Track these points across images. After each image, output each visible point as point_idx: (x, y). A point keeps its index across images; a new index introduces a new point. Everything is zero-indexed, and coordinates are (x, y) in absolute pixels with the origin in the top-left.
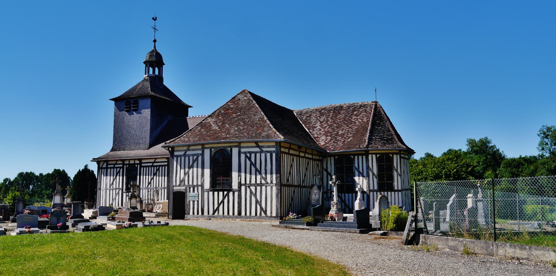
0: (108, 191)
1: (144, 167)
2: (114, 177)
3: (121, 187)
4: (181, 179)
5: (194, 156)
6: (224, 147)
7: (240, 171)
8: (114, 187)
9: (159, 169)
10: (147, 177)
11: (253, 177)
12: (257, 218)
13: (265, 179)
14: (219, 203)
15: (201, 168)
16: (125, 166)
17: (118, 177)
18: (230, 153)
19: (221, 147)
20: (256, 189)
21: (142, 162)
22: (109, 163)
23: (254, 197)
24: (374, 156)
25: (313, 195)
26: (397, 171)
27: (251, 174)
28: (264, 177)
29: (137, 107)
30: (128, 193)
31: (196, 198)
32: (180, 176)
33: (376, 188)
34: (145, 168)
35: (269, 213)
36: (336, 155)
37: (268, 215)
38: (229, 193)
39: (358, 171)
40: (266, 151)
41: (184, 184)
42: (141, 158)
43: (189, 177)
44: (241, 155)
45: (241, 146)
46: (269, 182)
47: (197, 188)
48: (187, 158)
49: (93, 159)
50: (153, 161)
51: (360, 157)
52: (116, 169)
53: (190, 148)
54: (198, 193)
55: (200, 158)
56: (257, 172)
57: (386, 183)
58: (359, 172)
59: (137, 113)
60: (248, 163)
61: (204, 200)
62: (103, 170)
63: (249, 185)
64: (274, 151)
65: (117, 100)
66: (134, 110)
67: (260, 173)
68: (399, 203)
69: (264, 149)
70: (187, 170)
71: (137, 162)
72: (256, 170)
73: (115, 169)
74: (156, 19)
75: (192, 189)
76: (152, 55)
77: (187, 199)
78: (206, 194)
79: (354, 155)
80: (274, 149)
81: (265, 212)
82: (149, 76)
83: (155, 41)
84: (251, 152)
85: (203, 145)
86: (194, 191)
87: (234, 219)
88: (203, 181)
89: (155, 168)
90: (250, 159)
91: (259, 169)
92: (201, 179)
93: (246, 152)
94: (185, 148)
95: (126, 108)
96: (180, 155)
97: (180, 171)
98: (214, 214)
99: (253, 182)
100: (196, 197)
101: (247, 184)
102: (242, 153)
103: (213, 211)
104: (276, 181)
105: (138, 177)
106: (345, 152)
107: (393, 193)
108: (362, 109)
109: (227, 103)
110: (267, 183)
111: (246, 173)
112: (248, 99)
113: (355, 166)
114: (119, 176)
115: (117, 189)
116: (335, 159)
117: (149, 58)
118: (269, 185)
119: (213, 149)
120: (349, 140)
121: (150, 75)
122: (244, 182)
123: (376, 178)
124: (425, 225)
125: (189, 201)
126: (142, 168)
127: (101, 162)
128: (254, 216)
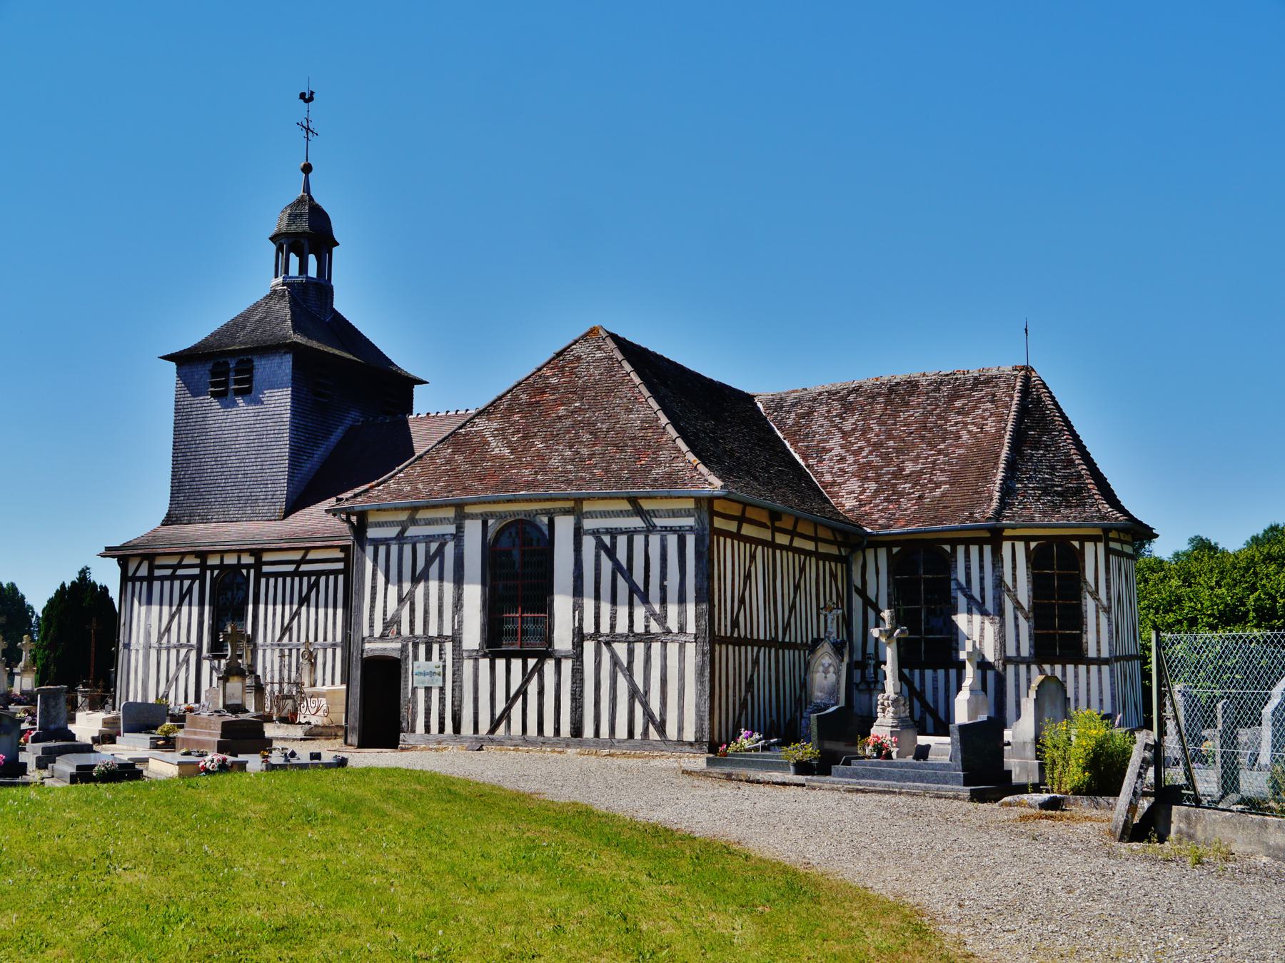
0: (153, 653)
1: (268, 575)
2: (174, 608)
3: (194, 640)
4: (389, 617)
5: (431, 542)
6: (528, 513)
7: (578, 592)
8: (174, 640)
9: (317, 584)
10: (279, 608)
11: (623, 611)
12: (634, 748)
13: (662, 619)
14: (512, 695)
15: (454, 582)
17: (185, 609)
18: (547, 532)
19: (518, 513)
20: (631, 653)
21: (264, 559)
22: (159, 561)
24: (1020, 546)
25: (818, 672)
27: (614, 601)
28: (658, 611)
29: (249, 381)
32: (385, 607)
33: (1025, 651)
34: (272, 581)
35: (672, 732)
36: (896, 543)
38: (543, 665)
39: (965, 595)
40: (665, 529)
41: (399, 633)
43: (412, 610)
46: (675, 630)
47: (440, 646)
48: (407, 549)
50: (297, 556)
51: (974, 550)
53: (418, 516)
54: (441, 664)
55: (450, 549)
56: (636, 597)
57: (1061, 635)
58: (970, 598)
59: (248, 403)
60: (606, 564)
61: (461, 687)
62: (138, 584)
63: (609, 639)
64: (691, 527)
65: (183, 360)
66: (239, 393)
67: (645, 600)
68: (1101, 701)
69: (659, 522)
70: (407, 586)
71: (247, 559)
72: (633, 589)
73: (177, 583)
74: (311, 99)
75: (422, 648)
76: (296, 215)
78: (468, 665)
79: (954, 543)
80: (690, 522)
81: (661, 728)
82: (289, 280)
83: (307, 169)
84: (616, 529)
85: (459, 506)
86: (429, 657)
87: (559, 749)
88: (460, 623)
89: (305, 579)
90: (611, 553)
91: (642, 587)
92: (453, 617)
93: (598, 530)
94: (403, 516)
95: (214, 385)
96: (386, 539)
97: (386, 589)
98: (493, 730)
99: (622, 627)
100: (437, 676)
101: (600, 636)
102: (588, 532)
104: (697, 626)
105: (250, 607)
106: (925, 532)
107: (1082, 668)
108: (982, 390)
109: (539, 370)
110: (668, 632)
111: (597, 597)
112: (606, 357)
113: (956, 580)
114: (190, 604)
115: (182, 646)
117: (288, 225)
118: (674, 638)
120: (938, 492)
121: (291, 277)
122: (593, 626)
123: (1027, 618)
125: (414, 689)
126: (263, 581)
128: (624, 741)
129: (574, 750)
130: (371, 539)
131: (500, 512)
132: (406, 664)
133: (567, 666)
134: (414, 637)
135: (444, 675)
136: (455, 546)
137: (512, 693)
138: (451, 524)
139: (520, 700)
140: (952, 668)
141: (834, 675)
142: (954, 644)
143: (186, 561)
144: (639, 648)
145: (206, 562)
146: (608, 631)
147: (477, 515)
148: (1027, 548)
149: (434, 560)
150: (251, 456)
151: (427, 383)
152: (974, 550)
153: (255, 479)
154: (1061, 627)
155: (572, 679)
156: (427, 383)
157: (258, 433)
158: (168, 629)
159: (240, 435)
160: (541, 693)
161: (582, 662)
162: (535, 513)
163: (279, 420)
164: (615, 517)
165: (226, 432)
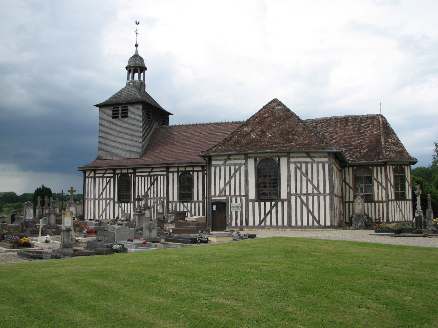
0: (97, 202)
1: (139, 176)
3: (112, 197)
5: (236, 165)
8: (104, 197)
9: (157, 179)
16: (116, 175)
20: (307, 199)
21: (137, 171)
24: (391, 167)
25: (356, 204)
29: (127, 113)
30: (120, 204)
31: (240, 209)
33: (393, 198)
34: (140, 178)
35: (322, 223)
36: (355, 166)
38: (277, 203)
39: (376, 181)
42: (135, 167)
45: (290, 156)
46: (322, 192)
55: (243, 168)
60: (299, 173)
62: (90, 179)
64: (327, 161)
69: (316, 160)
73: (105, 179)
75: (234, 199)
78: (250, 204)
80: (326, 159)
81: (318, 222)
83: (137, 46)
85: (246, 155)
86: (236, 201)
88: (248, 191)
89: (152, 177)
90: (300, 169)
99: (304, 191)
104: (330, 191)
107: (405, 202)
108: (369, 121)
110: (320, 193)
116: (353, 169)
119: (258, 159)
120: (365, 151)
123: (393, 188)
125: (231, 212)
126: (137, 178)
127: (116, 170)
129: (289, 230)
130: (213, 164)
131: (261, 156)
133: (286, 204)
135: (242, 207)
136: (245, 167)
137: (267, 212)
138: (243, 160)
139: (270, 215)
140: (347, 203)
142: (373, 195)
143: (107, 172)
144: (310, 198)
147: (252, 157)
148: (178, 174)
149: (306, 172)
151: (173, 114)
152: (379, 168)
156: (173, 114)
158: (102, 193)
159: (124, 131)
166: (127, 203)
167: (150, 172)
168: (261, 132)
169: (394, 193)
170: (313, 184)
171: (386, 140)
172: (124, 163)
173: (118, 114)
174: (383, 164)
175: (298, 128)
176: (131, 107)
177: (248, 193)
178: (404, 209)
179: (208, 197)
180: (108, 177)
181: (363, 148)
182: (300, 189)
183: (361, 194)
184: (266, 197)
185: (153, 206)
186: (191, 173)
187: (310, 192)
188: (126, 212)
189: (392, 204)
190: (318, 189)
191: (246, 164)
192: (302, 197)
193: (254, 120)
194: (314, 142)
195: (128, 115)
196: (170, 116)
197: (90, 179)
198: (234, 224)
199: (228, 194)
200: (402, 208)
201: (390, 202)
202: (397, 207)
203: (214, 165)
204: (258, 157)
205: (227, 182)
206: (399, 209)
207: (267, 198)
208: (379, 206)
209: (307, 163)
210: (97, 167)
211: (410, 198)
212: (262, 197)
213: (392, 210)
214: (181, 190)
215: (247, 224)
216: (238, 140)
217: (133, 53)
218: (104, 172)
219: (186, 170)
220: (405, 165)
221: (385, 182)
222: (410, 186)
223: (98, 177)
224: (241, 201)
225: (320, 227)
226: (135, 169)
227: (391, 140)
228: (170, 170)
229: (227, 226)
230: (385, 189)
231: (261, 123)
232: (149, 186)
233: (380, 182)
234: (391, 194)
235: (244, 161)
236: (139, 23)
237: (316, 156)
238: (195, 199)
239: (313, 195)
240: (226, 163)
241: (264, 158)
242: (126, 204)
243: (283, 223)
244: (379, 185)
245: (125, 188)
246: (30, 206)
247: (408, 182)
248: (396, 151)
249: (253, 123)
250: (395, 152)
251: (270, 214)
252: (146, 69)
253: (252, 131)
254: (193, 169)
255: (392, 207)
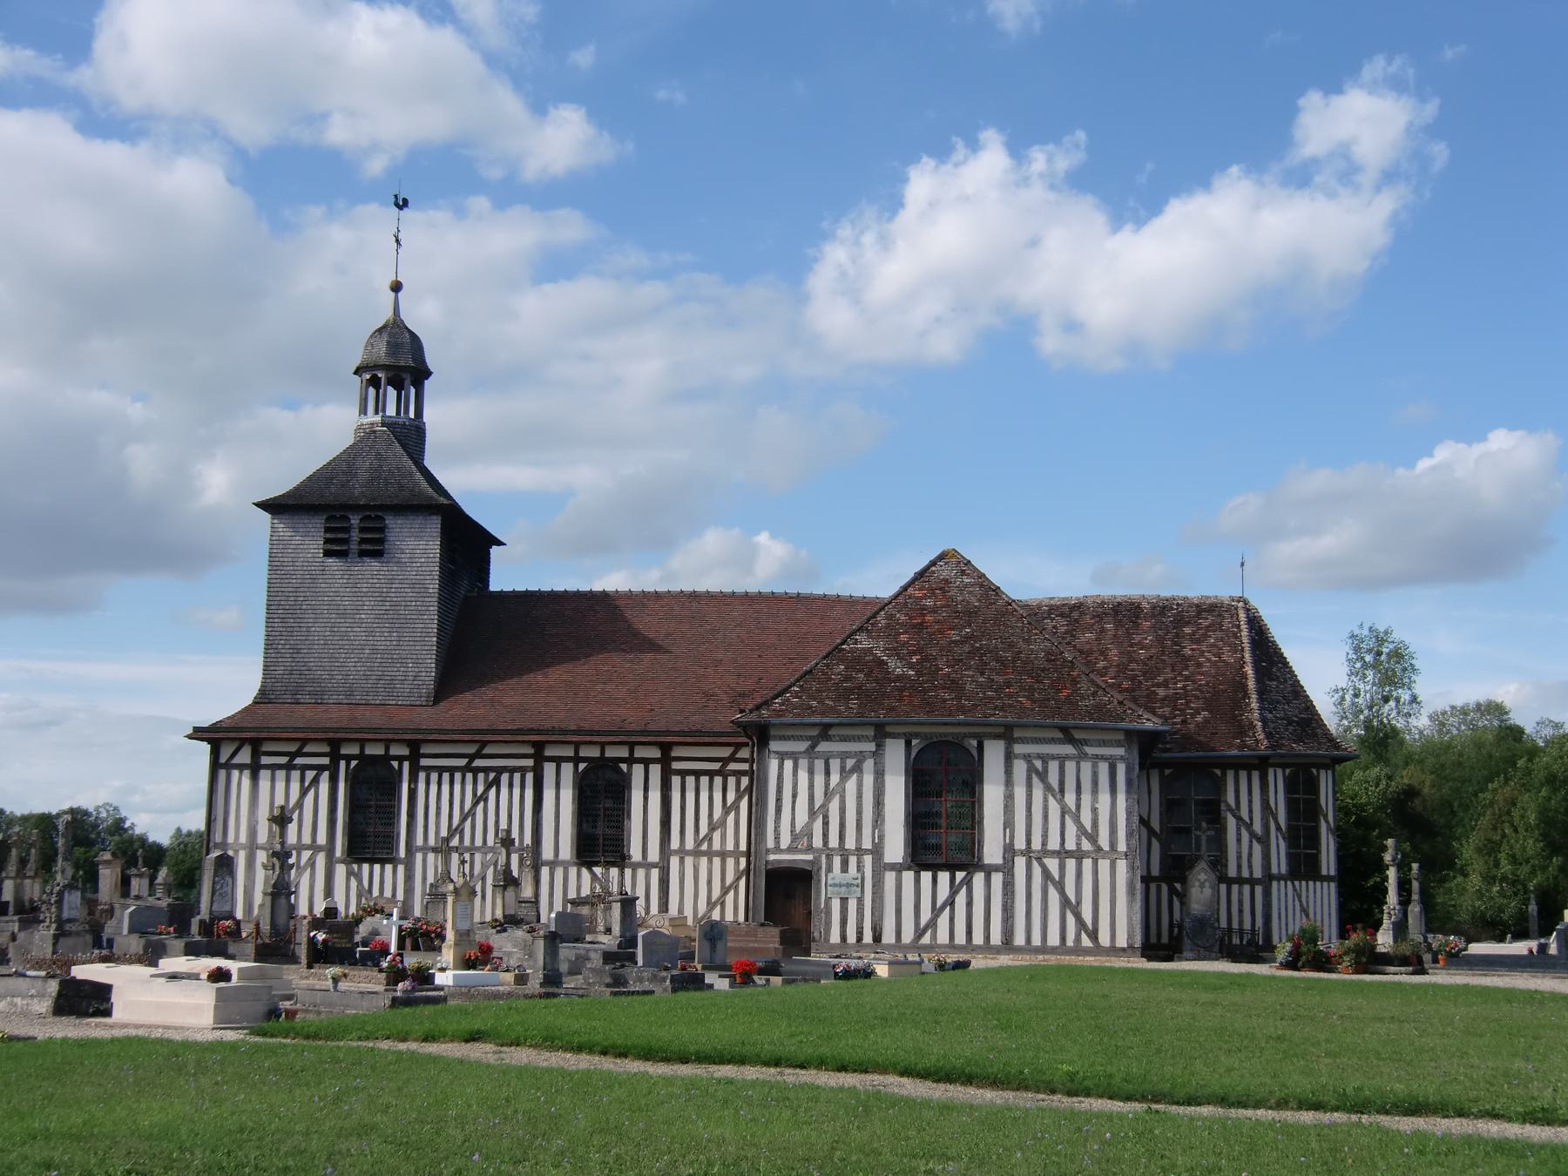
1: (428, 769)
3: (322, 839)
4: (798, 829)
5: (847, 757)
6: (957, 735)
9: (497, 782)
19: (945, 735)
20: (1062, 867)
23: (1056, 889)
24: (1279, 771)
25: (1194, 886)
26: (1326, 817)
29: (382, 541)
30: (355, 866)
31: (855, 892)
32: (793, 819)
33: (1284, 870)
35: (1104, 939)
37: (1102, 945)
38: (972, 877)
40: (1097, 757)
43: (826, 824)
44: (1015, 767)
45: (1015, 736)
46: (1106, 847)
49: (194, 728)
52: (436, 774)
54: (859, 875)
57: (1306, 854)
62: (235, 773)
64: (1122, 756)
69: (1090, 750)
71: (396, 750)
75: (837, 861)
77: (820, 892)
78: (890, 877)
80: (1120, 751)
81: (1094, 935)
82: (387, 420)
83: (397, 287)
87: (991, 956)
88: (881, 837)
90: (1043, 776)
96: (793, 753)
99: (1054, 844)
103: (916, 931)
104: (1128, 845)
108: (1207, 619)
110: (1099, 849)
113: (1226, 802)
119: (918, 741)
120: (1199, 719)
123: (1284, 838)
124: (366, 1031)
125: (828, 900)
126: (422, 775)
128: (1057, 948)
131: (925, 733)
132: (819, 876)
133: (997, 879)
134: (828, 849)
136: (875, 763)
137: (939, 904)
141: (1210, 890)
144: (1071, 864)
145: (339, 751)
146: (1039, 848)
147: (899, 734)
148: (576, 767)
150: (384, 629)
153: (389, 656)
154: (1305, 848)
155: (1003, 891)
157: (392, 603)
159: (368, 603)
160: (969, 904)
161: (1013, 875)
162: (963, 735)
163: (423, 590)
164: (1047, 743)
165: (346, 598)
166: (383, 862)
167: (472, 757)
168: (918, 657)
169: (1286, 854)
170: (1080, 822)
171: (1264, 684)
172: (375, 718)
173: (346, 541)
174: (1256, 762)
175: (1032, 650)
176: (399, 522)
177: (883, 843)
178: (1315, 906)
179: (756, 852)
180: (311, 767)
181: (1192, 709)
182: (1042, 836)
183: (1209, 856)
184: (936, 859)
185: (479, 874)
186: (624, 767)
187: (1071, 845)
188: (376, 893)
189: (1279, 890)
190: (1093, 838)
191: (878, 754)
192: (1047, 861)
193: (890, 617)
194: (1083, 698)
195: (387, 546)
196: (494, 550)
197: (235, 773)
198: (835, 938)
199: (821, 846)
200: (1307, 902)
201: (1275, 884)
202: (1294, 901)
203: (777, 753)
204: (917, 735)
205: (817, 807)
206: (1301, 905)
207: (940, 861)
208: (1240, 893)
209: (1062, 760)
210: (269, 729)
211: (1332, 873)
212: (930, 859)
213: (1280, 909)
214: (585, 826)
215: (877, 938)
216: (847, 679)
217: (387, 314)
218: (293, 748)
219: (581, 755)
220: (1320, 766)
221: (1262, 819)
222: (1333, 834)
223: (267, 767)
224: (860, 868)
225: (1097, 950)
226: (414, 746)
227: (1275, 683)
228: (549, 752)
229: (813, 945)
230: (1259, 840)
231: (914, 626)
232: (468, 805)
233: (1247, 819)
234: (1279, 858)
235: (871, 747)
236: (406, 202)
237: (1089, 740)
238: (635, 853)
239: (1079, 856)
240: (816, 750)
241: (935, 740)
242: (377, 867)
243: (987, 937)
244: (1242, 828)
245: (373, 810)
246: (225, 869)
247: (1327, 822)
248: (1294, 721)
249: (888, 626)
250: (1290, 723)
251: (948, 908)
252: (428, 374)
253: (895, 652)
254: (632, 752)
255: (1279, 900)
